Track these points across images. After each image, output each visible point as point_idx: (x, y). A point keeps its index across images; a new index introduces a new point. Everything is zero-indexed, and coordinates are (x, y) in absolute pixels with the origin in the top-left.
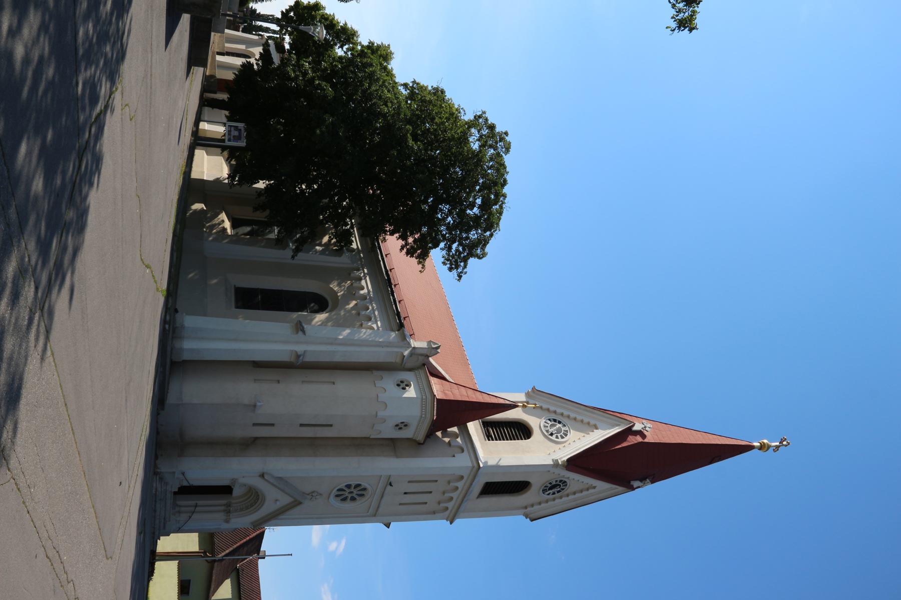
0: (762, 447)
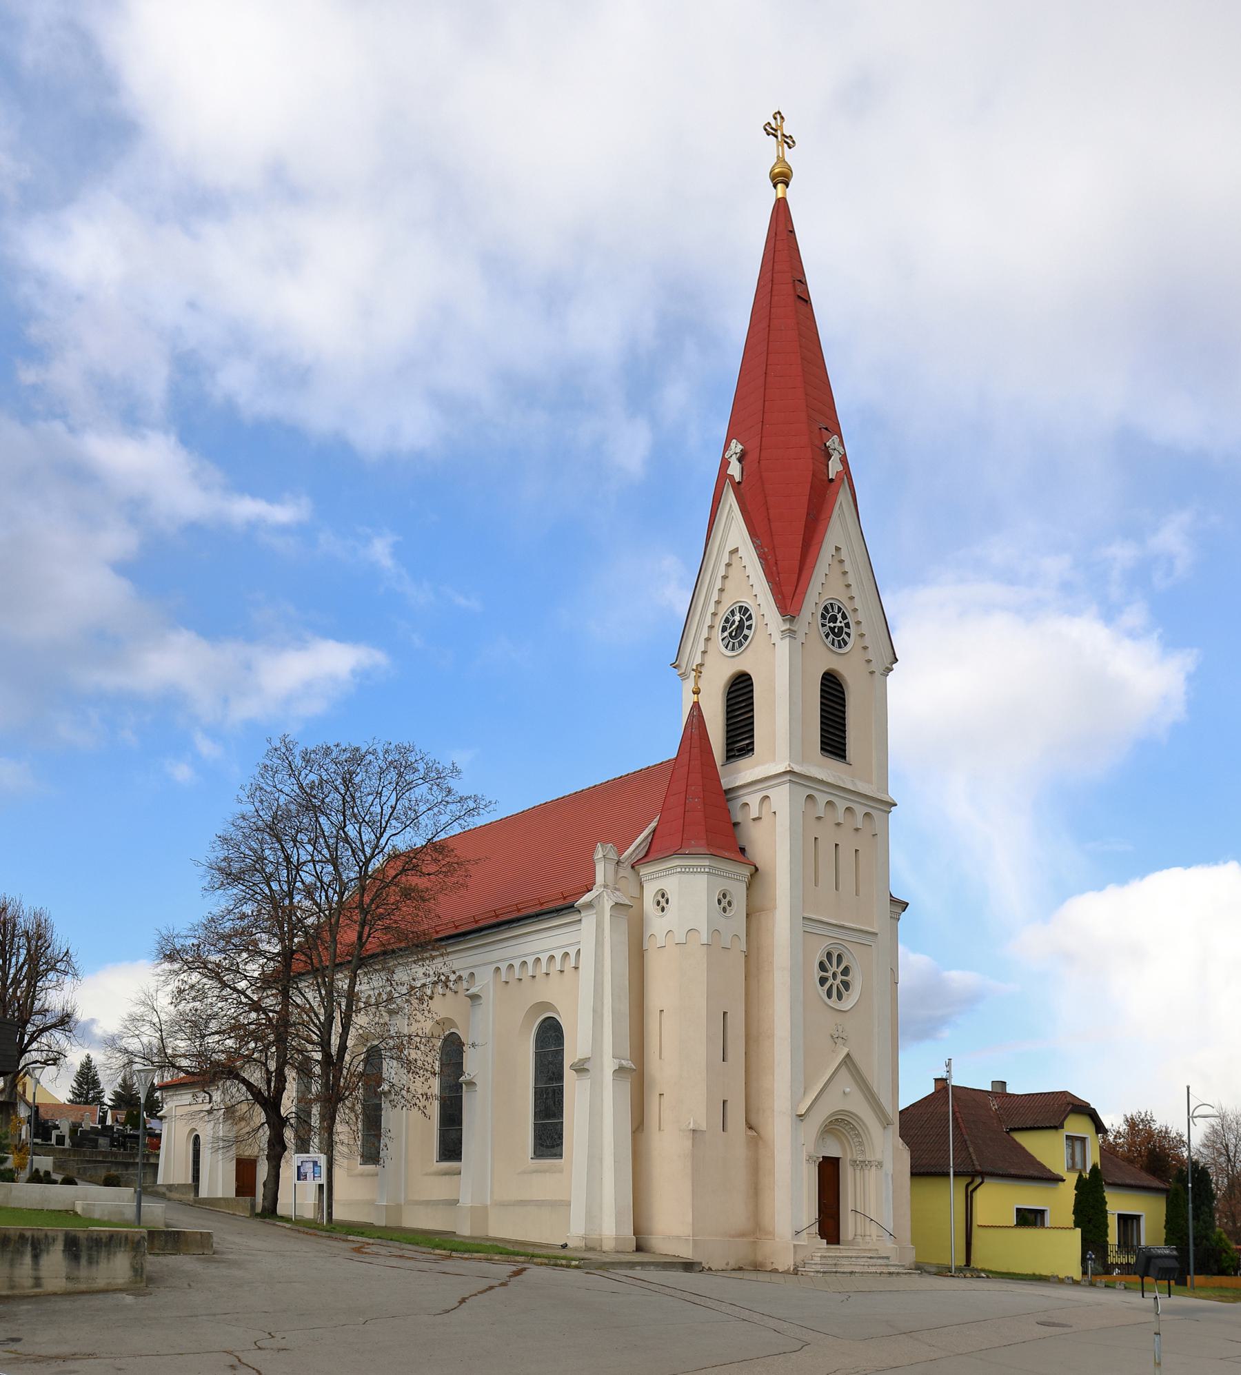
0: (781, 177)
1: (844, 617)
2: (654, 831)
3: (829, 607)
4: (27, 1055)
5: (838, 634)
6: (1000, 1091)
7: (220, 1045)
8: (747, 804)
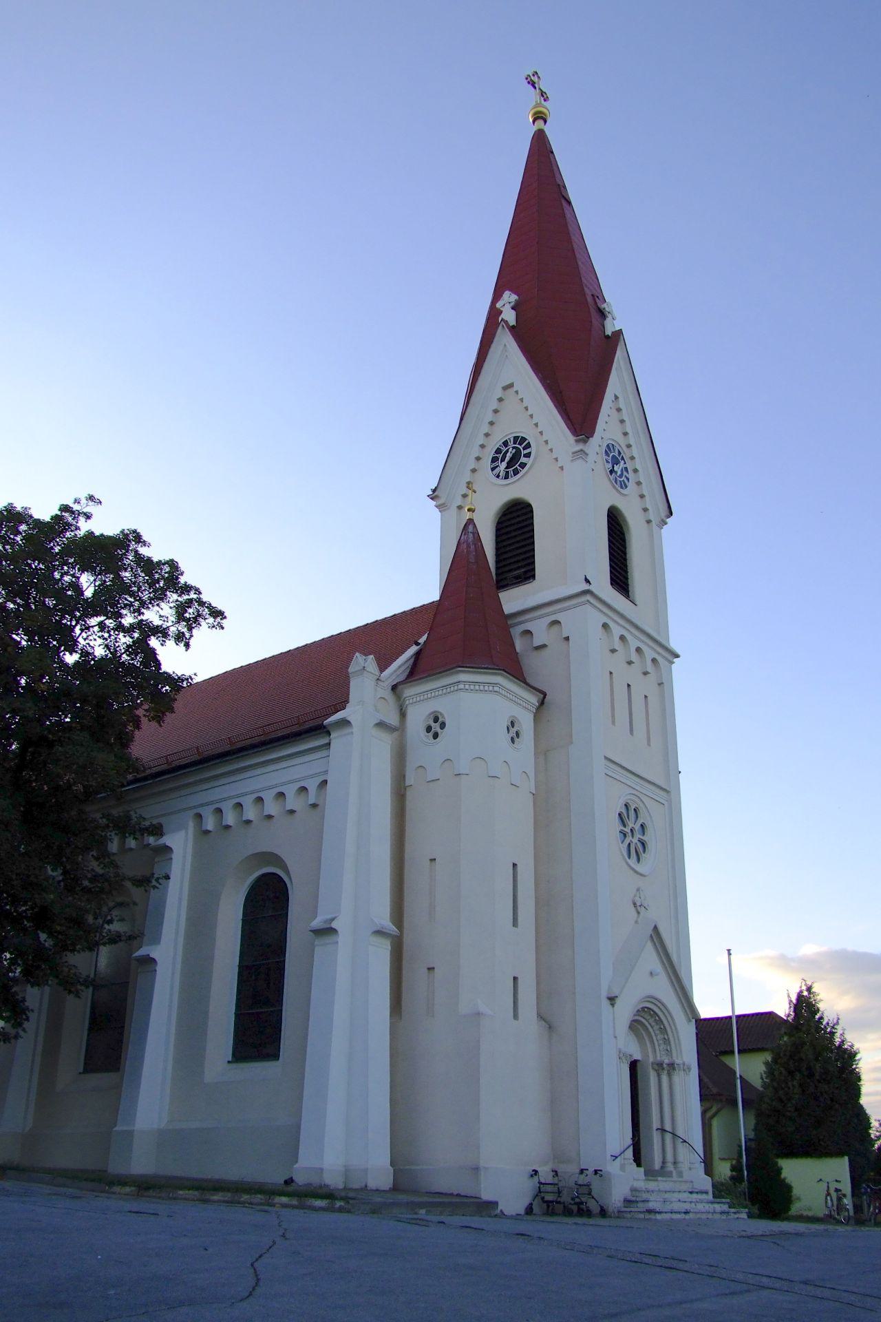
3: (611, 446)
8: (560, 622)
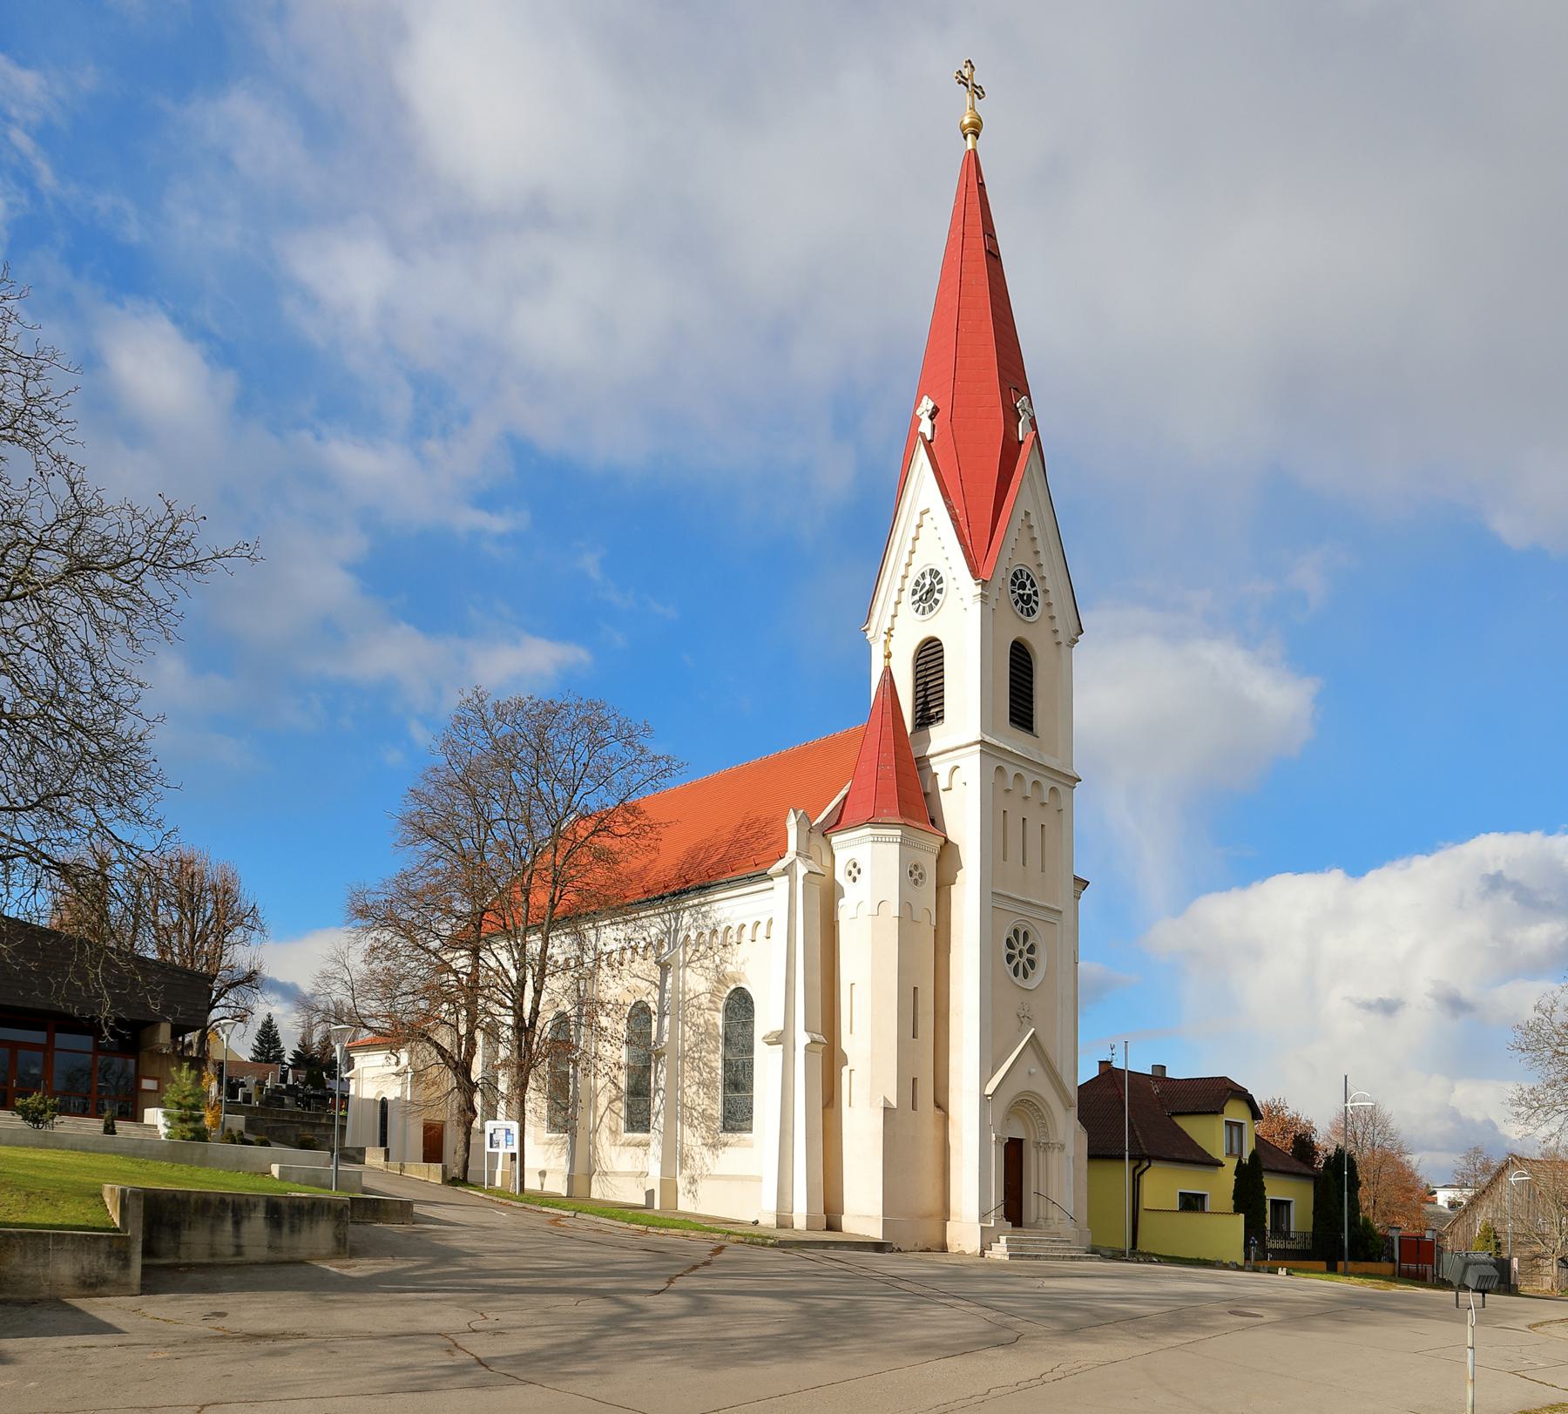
1: (1033, 585)
2: (845, 798)
3: (1018, 573)
4: (214, 1011)
5: (1027, 602)
6: (1160, 1075)
7: (409, 1006)
